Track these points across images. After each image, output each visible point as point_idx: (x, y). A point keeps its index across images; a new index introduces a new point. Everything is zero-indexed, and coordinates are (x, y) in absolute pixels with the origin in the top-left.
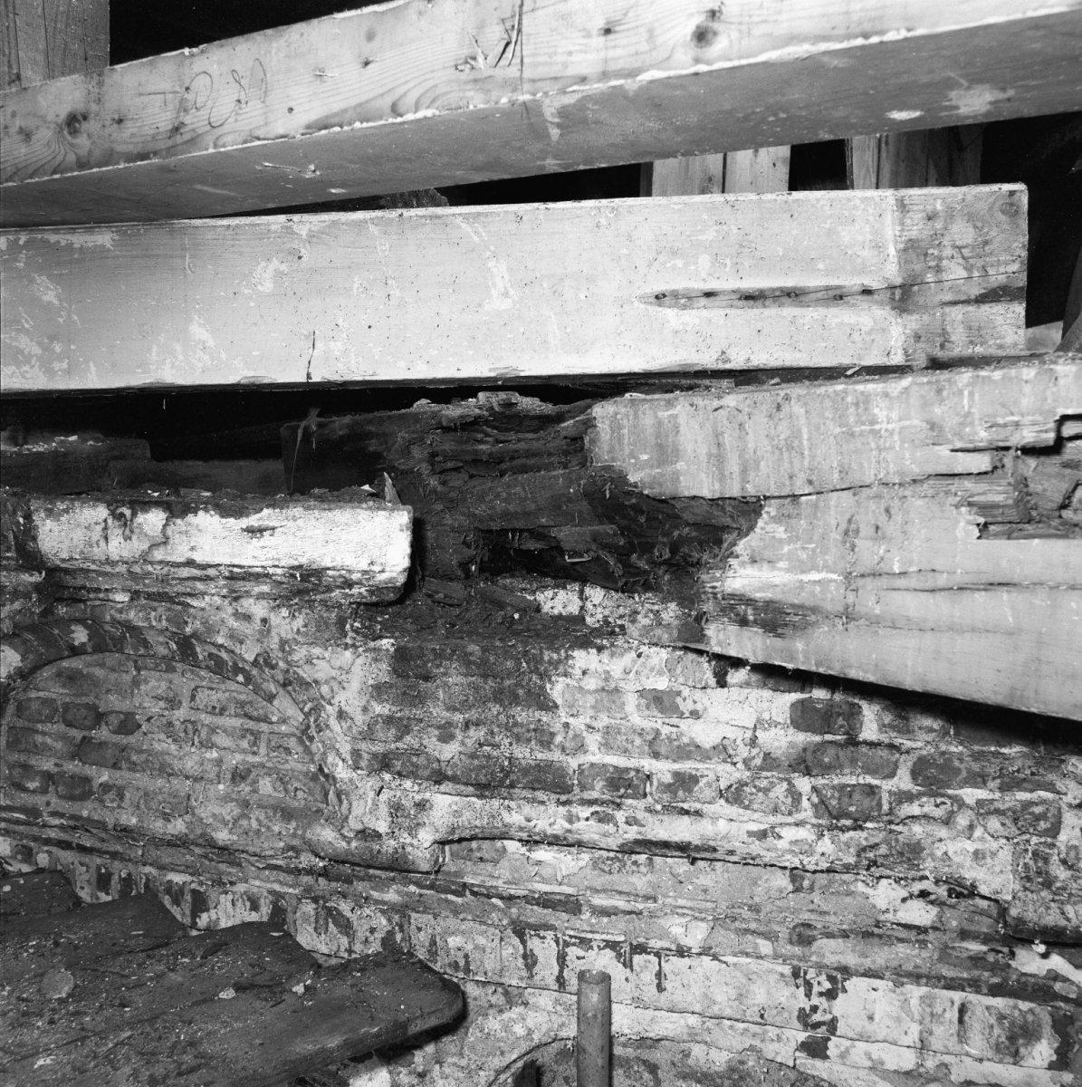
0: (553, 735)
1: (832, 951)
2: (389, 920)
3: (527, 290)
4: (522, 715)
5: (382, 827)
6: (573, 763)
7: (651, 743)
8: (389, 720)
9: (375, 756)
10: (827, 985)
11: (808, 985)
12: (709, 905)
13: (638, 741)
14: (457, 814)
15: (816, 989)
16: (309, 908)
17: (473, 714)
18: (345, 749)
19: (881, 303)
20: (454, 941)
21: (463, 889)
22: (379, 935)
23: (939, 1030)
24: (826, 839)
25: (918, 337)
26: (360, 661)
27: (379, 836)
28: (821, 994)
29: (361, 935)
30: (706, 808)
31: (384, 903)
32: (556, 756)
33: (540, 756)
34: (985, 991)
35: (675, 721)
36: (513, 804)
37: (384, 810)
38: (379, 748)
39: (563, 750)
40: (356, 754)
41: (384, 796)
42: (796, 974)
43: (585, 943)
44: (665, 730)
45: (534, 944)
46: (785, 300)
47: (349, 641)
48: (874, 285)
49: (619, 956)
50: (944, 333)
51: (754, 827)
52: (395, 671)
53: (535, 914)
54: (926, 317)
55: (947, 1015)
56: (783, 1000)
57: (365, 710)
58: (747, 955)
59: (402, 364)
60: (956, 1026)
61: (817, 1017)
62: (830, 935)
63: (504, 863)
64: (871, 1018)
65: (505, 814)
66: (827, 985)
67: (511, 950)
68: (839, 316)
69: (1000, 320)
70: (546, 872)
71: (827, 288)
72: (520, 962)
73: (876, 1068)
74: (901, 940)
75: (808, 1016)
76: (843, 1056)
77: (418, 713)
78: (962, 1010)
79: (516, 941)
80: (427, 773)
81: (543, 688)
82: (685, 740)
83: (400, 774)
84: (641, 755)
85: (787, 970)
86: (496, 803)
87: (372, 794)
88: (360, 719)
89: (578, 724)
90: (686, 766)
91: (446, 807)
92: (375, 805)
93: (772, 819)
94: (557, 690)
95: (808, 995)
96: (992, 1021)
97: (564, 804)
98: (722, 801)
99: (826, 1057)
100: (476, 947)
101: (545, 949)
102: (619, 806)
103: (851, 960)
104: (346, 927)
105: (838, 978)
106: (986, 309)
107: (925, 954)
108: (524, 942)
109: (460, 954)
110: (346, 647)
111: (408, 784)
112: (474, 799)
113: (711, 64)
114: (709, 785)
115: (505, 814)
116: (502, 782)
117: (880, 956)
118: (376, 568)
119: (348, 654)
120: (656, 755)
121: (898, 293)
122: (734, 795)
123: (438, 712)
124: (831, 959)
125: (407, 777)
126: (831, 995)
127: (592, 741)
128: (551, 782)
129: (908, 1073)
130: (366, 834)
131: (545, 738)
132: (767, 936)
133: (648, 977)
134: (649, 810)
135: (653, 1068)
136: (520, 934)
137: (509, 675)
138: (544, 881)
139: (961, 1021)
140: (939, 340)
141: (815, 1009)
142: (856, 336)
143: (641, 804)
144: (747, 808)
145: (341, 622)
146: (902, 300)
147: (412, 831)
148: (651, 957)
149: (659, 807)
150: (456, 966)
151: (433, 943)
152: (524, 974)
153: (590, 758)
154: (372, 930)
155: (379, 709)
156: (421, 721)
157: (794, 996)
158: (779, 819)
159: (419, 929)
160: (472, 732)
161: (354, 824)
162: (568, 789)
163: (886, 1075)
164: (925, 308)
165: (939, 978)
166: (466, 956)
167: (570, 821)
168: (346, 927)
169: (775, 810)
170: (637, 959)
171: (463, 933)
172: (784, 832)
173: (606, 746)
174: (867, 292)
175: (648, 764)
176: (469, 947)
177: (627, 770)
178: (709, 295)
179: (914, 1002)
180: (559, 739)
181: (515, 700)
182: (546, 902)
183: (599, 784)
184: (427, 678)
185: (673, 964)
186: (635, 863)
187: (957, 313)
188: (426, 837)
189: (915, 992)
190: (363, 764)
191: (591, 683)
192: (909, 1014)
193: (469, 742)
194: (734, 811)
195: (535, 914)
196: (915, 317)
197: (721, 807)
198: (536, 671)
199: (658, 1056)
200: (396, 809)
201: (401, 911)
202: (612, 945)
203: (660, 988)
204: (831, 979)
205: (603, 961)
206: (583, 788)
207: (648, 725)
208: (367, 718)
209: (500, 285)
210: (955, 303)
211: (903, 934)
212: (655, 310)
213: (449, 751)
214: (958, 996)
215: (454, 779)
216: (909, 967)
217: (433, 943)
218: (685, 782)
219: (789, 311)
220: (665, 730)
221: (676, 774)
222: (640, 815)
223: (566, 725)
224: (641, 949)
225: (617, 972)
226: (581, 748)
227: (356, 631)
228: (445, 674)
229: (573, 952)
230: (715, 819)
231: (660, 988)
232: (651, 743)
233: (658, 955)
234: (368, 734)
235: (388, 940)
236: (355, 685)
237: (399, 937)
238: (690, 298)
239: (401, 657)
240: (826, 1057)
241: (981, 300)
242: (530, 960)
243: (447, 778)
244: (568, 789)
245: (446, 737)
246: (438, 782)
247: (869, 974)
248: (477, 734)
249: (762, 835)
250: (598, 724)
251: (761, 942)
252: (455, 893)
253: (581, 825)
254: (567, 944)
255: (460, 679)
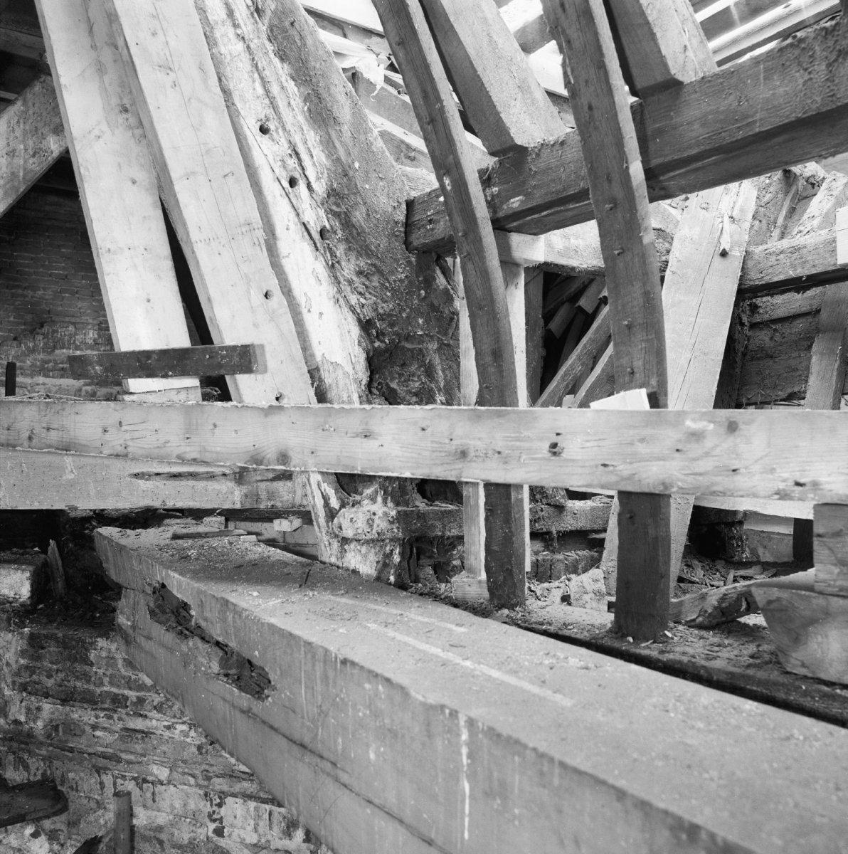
0: (90, 677)
1: (220, 784)
2: (45, 764)
3: (81, 470)
4: (79, 667)
5: (22, 719)
6: (98, 691)
7: (128, 683)
8: (27, 667)
9: (22, 684)
10: (218, 801)
11: (211, 800)
12: (166, 760)
13: (123, 682)
14: (52, 713)
15: (214, 802)
16: (11, 757)
17: (60, 666)
18: (9, 680)
19: (231, 480)
20: (71, 775)
21: (71, 750)
22: (40, 772)
23: (261, 824)
24: (193, 731)
25: (246, 496)
26: (15, 639)
27: (21, 723)
28: (216, 805)
29: (32, 772)
30: (149, 714)
31: (41, 755)
32: (92, 687)
33: (85, 686)
34: (703, 836)
35: (137, 673)
36: (74, 709)
37: (23, 710)
38: (22, 681)
39: (95, 684)
40: (14, 683)
41: (23, 704)
42: (206, 795)
43: (124, 777)
44: (133, 677)
45: (104, 777)
46: (190, 477)
47: (12, 628)
48: (228, 471)
49: (137, 784)
50: (258, 495)
51: (166, 724)
52: (29, 644)
53: (102, 762)
54: (250, 487)
55: (264, 816)
56: (201, 807)
57: (17, 662)
58: (185, 784)
59: (28, 502)
60: (268, 822)
61: (215, 816)
62: (218, 777)
63: (84, 737)
64: (235, 817)
65: (71, 714)
66: (218, 801)
67: (94, 780)
68: (212, 486)
69: (281, 489)
70: (101, 741)
71: (207, 473)
72: (98, 786)
73: (242, 842)
74: (244, 779)
75: (212, 816)
76: (229, 836)
77: (39, 664)
78: (270, 814)
79: (96, 775)
80: (41, 693)
81: (86, 655)
82: (141, 682)
83: (30, 693)
84: (125, 688)
85: (202, 792)
86: (68, 708)
87: (18, 703)
88: (14, 666)
89: (101, 672)
90: (142, 694)
91: (48, 708)
92: (20, 707)
93: (173, 720)
94: (92, 655)
95: (211, 805)
96: (281, 819)
97: (94, 709)
98: (155, 711)
99: (224, 837)
100: (80, 778)
101: (108, 779)
102: (116, 711)
103: (225, 788)
104: (26, 767)
105: (223, 795)
106: (275, 484)
107: (254, 786)
108: (99, 776)
109: (74, 782)
110: (10, 631)
111: (33, 698)
112: (59, 706)
113: (468, 127)
114: (149, 703)
115: (71, 714)
116: (71, 698)
117: (238, 787)
118: (17, 597)
119: (10, 635)
120: (130, 689)
121: (237, 476)
122: (159, 708)
123: (46, 663)
124: (218, 788)
125: (33, 695)
126: (220, 805)
127: (106, 680)
128: (90, 700)
129: (255, 845)
130: (16, 722)
131: (86, 677)
132: (193, 776)
133: (149, 795)
134: (127, 714)
135: (161, 842)
136: (98, 772)
137: (74, 648)
138: (101, 746)
139: (270, 819)
140: (255, 498)
141: (214, 812)
142: (220, 496)
143: (124, 711)
144: (164, 714)
145: (9, 620)
146: (239, 479)
147: (35, 721)
148: (150, 785)
149: (132, 713)
150: (71, 788)
151: (63, 776)
152: (100, 792)
153: (105, 688)
154: (38, 769)
155: (22, 661)
156: (39, 668)
157: (205, 806)
158: (176, 720)
159: (57, 769)
160: (59, 675)
161: (11, 717)
162: (96, 703)
163: (247, 846)
164: (249, 483)
165: (259, 798)
166: (76, 783)
167: (97, 718)
168: (26, 767)
169: (175, 717)
170: (145, 785)
171: (75, 771)
172: (177, 726)
173: (111, 683)
174: (224, 475)
175: (126, 692)
176: (78, 778)
177: (118, 695)
178: (158, 474)
179: (252, 809)
180: (93, 679)
181: (76, 660)
182: (104, 756)
183: (108, 701)
184: (43, 648)
185: (159, 788)
186: (137, 738)
187: (263, 485)
188: (40, 724)
189: (252, 805)
190: (16, 688)
191: (104, 654)
192: (250, 815)
193: (58, 679)
194: (159, 716)
195: (102, 762)
196: (245, 487)
197: (154, 714)
198: (83, 647)
199: (163, 837)
200: (28, 710)
201: (48, 759)
202: (134, 779)
203: (154, 801)
204: (220, 797)
205: (130, 786)
206: (102, 703)
207: (126, 674)
208: (17, 666)
209: (69, 468)
210: (262, 481)
211: (244, 776)
212: (134, 480)
213: (50, 683)
214: (268, 807)
215: (52, 696)
216: (248, 792)
217: (63, 776)
218: (141, 701)
219: (191, 483)
220: (133, 677)
221: (138, 698)
222: (124, 716)
223: (96, 673)
224: (145, 781)
225: (136, 793)
226: (102, 684)
227: (15, 624)
228: (49, 646)
229: (119, 781)
230: (151, 719)
231: (154, 801)
232: (128, 683)
233: (153, 784)
234: (18, 674)
235: (44, 774)
236: (13, 650)
237: (49, 772)
238: (150, 476)
239: (32, 637)
240: (224, 837)
241: (273, 480)
242: (102, 785)
243: (50, 696)
244: (96, 703)
245: (49, 676)
246: (47, 698)
247: (234, 795)
248: (61, 675)
249: (168, 728)
250: (108, 673)
251: (190, 778)
252: (68, 751)
253: (100, 720)
254: (117, 778)
255: (55, 649)
